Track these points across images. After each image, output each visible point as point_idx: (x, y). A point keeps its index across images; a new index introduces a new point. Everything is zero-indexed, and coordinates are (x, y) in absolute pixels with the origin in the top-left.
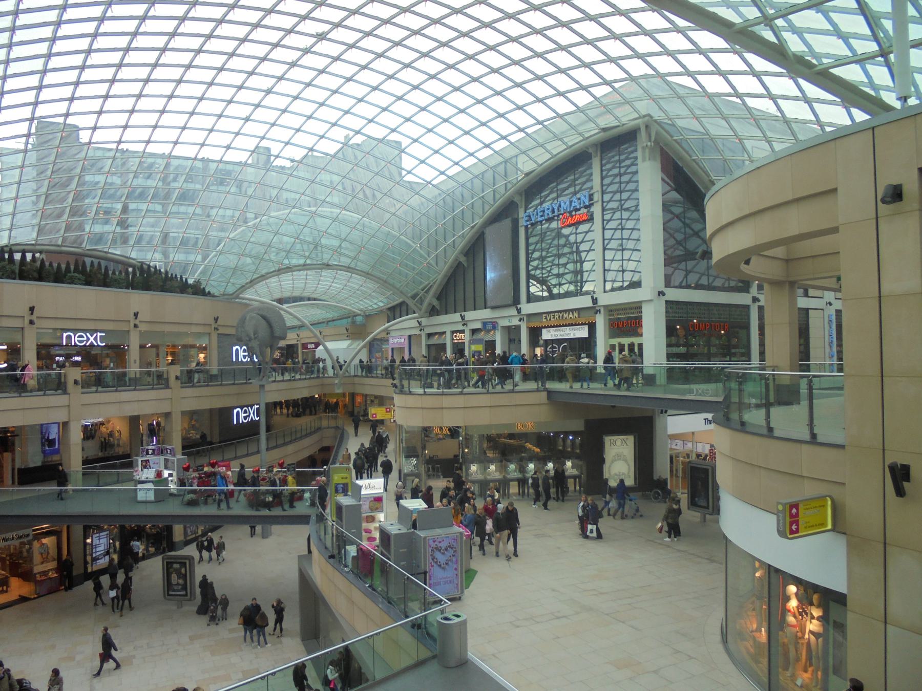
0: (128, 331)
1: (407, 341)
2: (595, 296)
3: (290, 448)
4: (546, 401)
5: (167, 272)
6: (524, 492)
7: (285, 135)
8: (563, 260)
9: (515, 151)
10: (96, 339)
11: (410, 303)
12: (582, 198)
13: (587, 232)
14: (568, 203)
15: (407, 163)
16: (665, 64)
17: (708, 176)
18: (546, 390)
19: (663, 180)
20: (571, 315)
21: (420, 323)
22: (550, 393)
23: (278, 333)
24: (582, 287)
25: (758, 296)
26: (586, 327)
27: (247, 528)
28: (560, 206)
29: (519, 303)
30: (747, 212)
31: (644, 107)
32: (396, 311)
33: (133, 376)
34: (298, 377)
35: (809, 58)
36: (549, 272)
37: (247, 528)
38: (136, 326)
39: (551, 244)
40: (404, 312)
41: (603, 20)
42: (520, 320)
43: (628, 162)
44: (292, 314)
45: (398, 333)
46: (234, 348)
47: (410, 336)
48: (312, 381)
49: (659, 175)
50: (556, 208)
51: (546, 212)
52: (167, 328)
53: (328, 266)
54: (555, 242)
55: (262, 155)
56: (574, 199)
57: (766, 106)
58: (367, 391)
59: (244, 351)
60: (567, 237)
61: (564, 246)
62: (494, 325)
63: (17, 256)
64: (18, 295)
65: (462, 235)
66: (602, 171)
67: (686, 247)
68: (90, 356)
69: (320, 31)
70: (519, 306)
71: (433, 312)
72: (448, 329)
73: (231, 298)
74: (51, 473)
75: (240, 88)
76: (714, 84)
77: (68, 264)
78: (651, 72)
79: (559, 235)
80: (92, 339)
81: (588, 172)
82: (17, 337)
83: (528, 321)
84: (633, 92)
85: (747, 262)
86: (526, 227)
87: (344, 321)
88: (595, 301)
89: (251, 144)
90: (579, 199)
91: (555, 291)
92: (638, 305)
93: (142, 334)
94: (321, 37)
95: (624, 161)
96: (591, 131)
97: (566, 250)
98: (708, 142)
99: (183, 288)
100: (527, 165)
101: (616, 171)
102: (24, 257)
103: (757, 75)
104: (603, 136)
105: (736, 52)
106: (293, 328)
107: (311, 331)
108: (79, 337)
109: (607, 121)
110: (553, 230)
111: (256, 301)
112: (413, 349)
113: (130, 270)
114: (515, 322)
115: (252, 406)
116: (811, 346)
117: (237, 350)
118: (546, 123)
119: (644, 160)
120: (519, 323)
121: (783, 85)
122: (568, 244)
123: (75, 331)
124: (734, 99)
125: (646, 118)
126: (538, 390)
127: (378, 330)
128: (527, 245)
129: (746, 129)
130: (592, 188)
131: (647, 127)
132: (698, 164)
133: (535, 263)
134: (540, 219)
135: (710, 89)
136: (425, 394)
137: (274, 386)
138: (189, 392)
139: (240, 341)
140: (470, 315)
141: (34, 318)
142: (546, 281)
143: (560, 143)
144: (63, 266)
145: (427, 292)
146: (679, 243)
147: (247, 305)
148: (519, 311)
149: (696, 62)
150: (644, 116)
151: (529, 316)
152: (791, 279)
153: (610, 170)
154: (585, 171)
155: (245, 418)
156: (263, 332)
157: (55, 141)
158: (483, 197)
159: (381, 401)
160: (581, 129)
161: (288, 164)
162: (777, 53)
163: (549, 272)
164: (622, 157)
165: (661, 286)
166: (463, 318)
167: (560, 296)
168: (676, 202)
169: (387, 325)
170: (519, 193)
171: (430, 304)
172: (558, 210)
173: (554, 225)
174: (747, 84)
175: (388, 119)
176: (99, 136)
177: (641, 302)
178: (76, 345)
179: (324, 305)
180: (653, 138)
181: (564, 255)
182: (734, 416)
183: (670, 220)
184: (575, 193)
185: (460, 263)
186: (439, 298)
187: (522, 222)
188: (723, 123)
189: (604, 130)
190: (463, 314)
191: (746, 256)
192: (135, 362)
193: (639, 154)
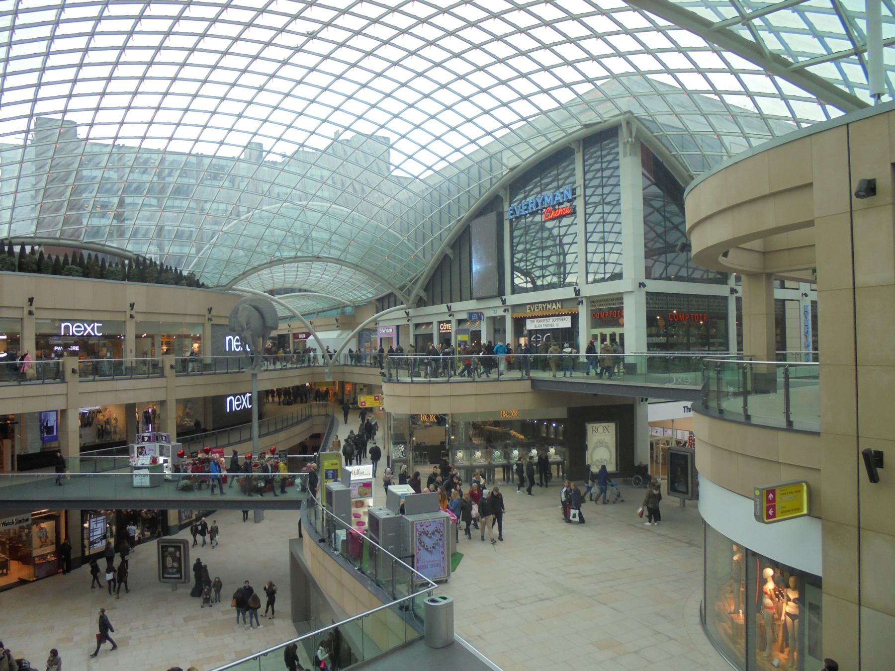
0: (125, 322)
1: (395, 331)
2: (577, 288)
3: (282, 435)
4: (530, 389)
5: (162, 264)
6: (508, 477)
7: (277, 131)
8: (547, 253)
9: (500, 147)
10: (93, 329)
11: (398, 294)
12: (565, 192)
13: (570, 226)
14: (551, 197)
15: (395, 158)
16: (645, 63)
17: (688, 171)
18: (530, 378)
19: (643, 174)
20: (554, 306)
21: (407, 314)
22: (534, 382)
23: (270, 323)
24: (565, 279)
25: (735, 287)
26: (569, 318)
27: (240, 513)
28: (543, 200)
29: (504, 294)
30: (725, 206)
31: (625, 104)
32: (384, 302)
33: (129, 365)
34: (289, 366)
35: (785, 57)
36: (533, 264)
37: (240, 513)
38: (132, 317)
39: (535, 236)
40: (392, 303)
42: (505, 311)
43: (609, 158)
44: (284, 305)
45: (386, 324)
46: (228, 338)
47: (398, 326)
48: (303, 370)
49: (639, 170)
50: (539, 202)
51: (530, 206)
52: (162, 319)
53: (318, 258)
54: (539, 235)
55: (255, 150)
56: (557, 193)
57: (743, 102)
58: (357, 379)
59: (237, 341)
60: (550, 230)
61: (548, 239)
62: (480, 316)
63: (17, 249)
64: (17, 286)
65: (449, 229)
66: (584, 166)
67: (665, 240)
68: (87, 346)
69: (311, 30)
70: (504, 297)
71: (420, 303)
72: (435, 320)
73: (224, 290)
76: (694, 82)
77: (66, 256)
78: (632, 70)
79: (543, 228)
80: (89, 329)
81: (571, 167)
82: (17, 328)
83: (513, 312)
84: (615, 89)
85: (725, 255)
86: (511, 220)
87: (334, 312)
88: (577, 292)
89: (244, 139)
90: (562, 193)
91: (539, 282)
92: (619, 296)
93: (138, 324)
94: (312, 36)
95: (606, 156)
96: (574, 127)
97: (550, 243)
98: (688, 138)
99: (178, 279)
100: (511, 161)
101: (598, 166)
102: (23, 249)
103: (735, 73)
104: (585, 132)
105: (714, 51)
106: (284, 318)
107: (302, 321)
108: (77, 327)
109: (589, 117)
110: (536, 223)
111: (248, 292)
112: (401, 339)
113: (127, 262)
114: (500, 312)
115: (244, 395)
116: (787, 336)
117: (230, 340)
118: (530, 120)
119: (625, 156)
120: (503, 314)
121: (760, 82)
122: (551, 237)
123: (73, 321)
124: (712, 96)
125: (627, 115)
126: (522, 379)
127: (366, 321)
128: (512, 238)
130: (574, 183)
131: (628, 123)
132: (677, 159)
133: (519, 256)
134: (524, 213)
135: (690, 87)
136: (412, 382)
137: (266, 375)
138: (184, 380)
139: (233, 332)
140: (456, 306)
141: (33, 308)
142: (530, 273)
143: (544, 138)
144: (62, 259)
145: (415, 283)
146: (659, 236)
147: (239, 296)
148: (504, 302)
149: (675, 61)
150: (626, 113)
151: (514, 306)
152: (768, 271)
153: (592, 165)
154: (568, 166)
155: (238, 406)
156: (256, 322)
157: (53, 137)
158: (469, 191)
159: (370, 389)
160: (564, 125)
161: (279, 159)
162: (754, 51)
163: (533, 264)
164: (604, 153)
165: (642, 278)
166: (449, 308)
167: (543, 288)
168: (656, 197)
169: (376, 315)
170: (503, 187)
171: (417, 295)
172: (542, 204)
173: (538, 218)
174: (725, 82)
175: (377, 116)
176: (96, 132)
177: (622, 293)
178: (74, 335)
179: (314, 297)
180: (634, 134)
181: (548, 247)
182: (713, 404)
183: (650, 214)
184: (558, 188)
185: (446, 255)
186: (426, 289)
187: (507, 216)
188: (702, 119)
189: (586, 126)
190: (449, 305)
191: (724, 249)
192: (131, 351)
193: (620, 149)
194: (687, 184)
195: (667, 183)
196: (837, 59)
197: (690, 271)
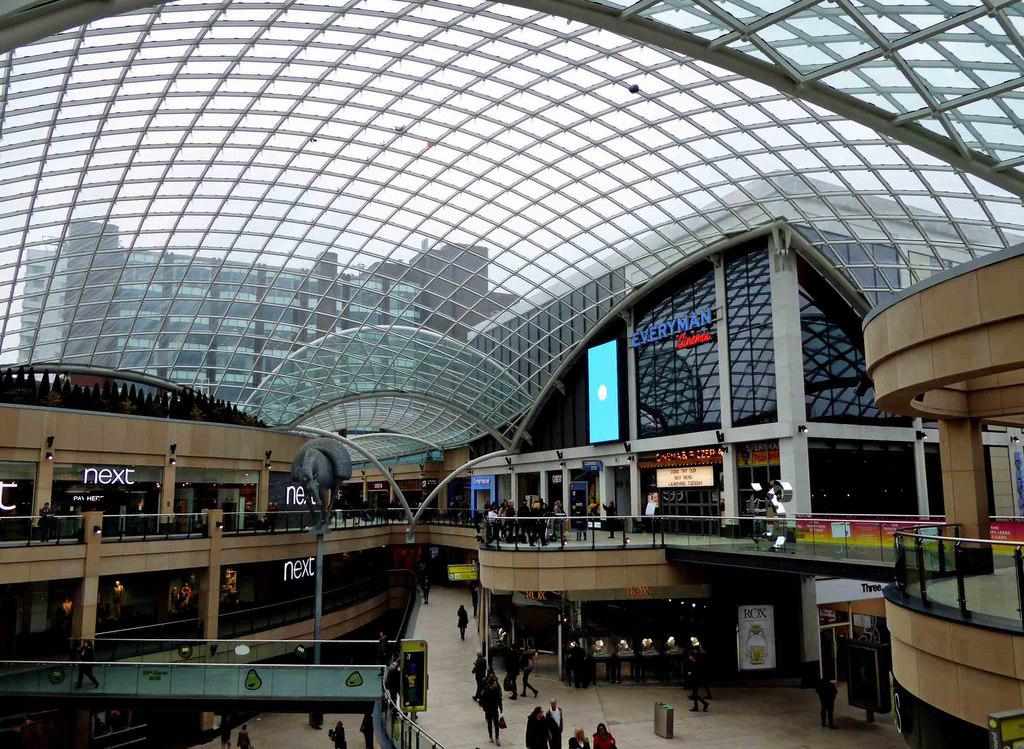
0: (163, 467)
1: (493, 481)
2: (721, 432)
3: (351, 612)
4: (665, 562)
5: (212, 398)
6: (637, 673)
7: (356, 242)
8: (680, 387)
9: (623, 262)
10: (123, 477)
11: (498, 436)
12: (703, 315)
13: (707, 354)
15: (494, 274)
16: (802, 160)
17: (856, 287)
18: (663, 546)
19: (800, 293)
21: (509, 461)
23: (341, 472)
25: (923, 431)
27: (305, 718)
28: (676, 324)
30: (921, 339)
31: (778, 209)
32: (482, 446)
33: (165, 522)
34: (362, 523)
35: (980, 150)
36: (663, 400)
37: (305, 718)
39: (665, 367)
41: (663, 99)
43: (756, 272)
44: (357, 448)
45: (481, 473)
46: (289, 489)
47: (497, 477)
48: (378, 529)
49: (796, 287)
50: (672, 326)
51: (660, 331)
52: (209, 464)
54: (671, 365)
55: (327, 262)
56: (693, 316)
57: (928, 205)
58: (447, 542)
59: (300, 492)
60: (683, 360)
61: (680, 370)
63: (39, 377)
64: (34, 422)
66: (726, 282)
67: (836, 374)
68: (113, 497)
69: (400, 126)
70: (628, 443)
71: (524, 448)
72: (542, 470)
73: (284, 432)
74: (60, 638)
75: (273, 184)
76: (863, 181)
77: (97, 387)
78: (785, 168)
79: (675, 357)
80: (118, 476)
81: (710, 283)
84: (760, 190)
85: (920, 398)
86: (636, 349)
87: (418, 458)
88: (721, 437)
89: (316, 251)
90: (699, 316)
91: (671, 423)
94: (401, 132)
95: (751, 270)
96: (713, 237)
97: (683, 374)
98: (853, 248)
99: (230, 416)
100: (635, 277)
101: (742, 282)
102: (46, 378)
103: (916, 170)
104: (727, 242)
105: (889, 144)
106: (358, 463)
107: (378, 467)
109: (732, 225)
110: (667, 352)
111: (315, 432)
112: (501, 491)
113: (169, 394)
114: (624, 461)
115: (306, 559)
116: (995, 492)
121: (946, 180)
122: (685, 367)
123: (99, 466)
124: (887, 197)
127: (459, 469)
128: (638, 368)
129: (815, 210)
131: (781, 232)
132: (842, 273)
133: (645, 390)
134: (652, 339)
135: (857, 186)
136: (517, 550)
137: (334, 536)
138: (232, 542)
139: (296, 481)
140: (568, 453)
142: (660, 411)
143: (676, 251)
144: (91, 389)
145: (518, 424)
146: (821, 367)
147: (305, 438)
148: (628, 448)
149: (839, 156)
151: (640, 454)
152: (975, 415)
153: (735, 280)
154: (705, 283)
155: (298, 573)
156: (324, 470)
157: (92, 249)
158: (584, 314)
159: (465, 556)
160: (701, 235)
161: (356, 273)
162: (950, 151)
163: (663, 400)
164: (750, 266)
165: (802, 418)
166: (560, 456)
168: (814, 318)
169: (470, 462)
170: (628, 309)
173: (669, 345)
174: (903, 181)
175: (474, 225)
176: (143, 242)
179: (396, 438)
180: (788, 246)
181: (681, 381)
182: (914, 589)
183: (809, 340)
184: (694, 308)
185: (557, 391)
187: (631, 343)
188: (874, 225)
189: (729, 236)
190: (560, 451)
191: (919, 392)
192: (169, 504)
193: (771, 261)
194: (865, 313)
195: (835, 309)
196: (853, 65)
197: (857, 402)
